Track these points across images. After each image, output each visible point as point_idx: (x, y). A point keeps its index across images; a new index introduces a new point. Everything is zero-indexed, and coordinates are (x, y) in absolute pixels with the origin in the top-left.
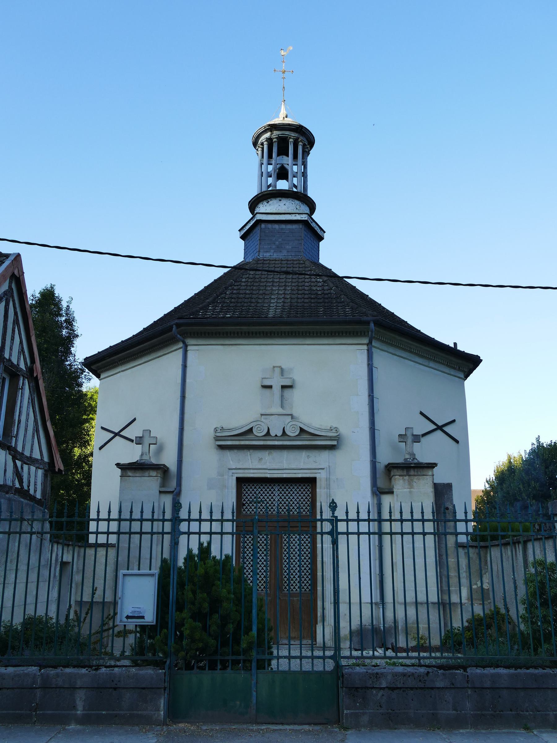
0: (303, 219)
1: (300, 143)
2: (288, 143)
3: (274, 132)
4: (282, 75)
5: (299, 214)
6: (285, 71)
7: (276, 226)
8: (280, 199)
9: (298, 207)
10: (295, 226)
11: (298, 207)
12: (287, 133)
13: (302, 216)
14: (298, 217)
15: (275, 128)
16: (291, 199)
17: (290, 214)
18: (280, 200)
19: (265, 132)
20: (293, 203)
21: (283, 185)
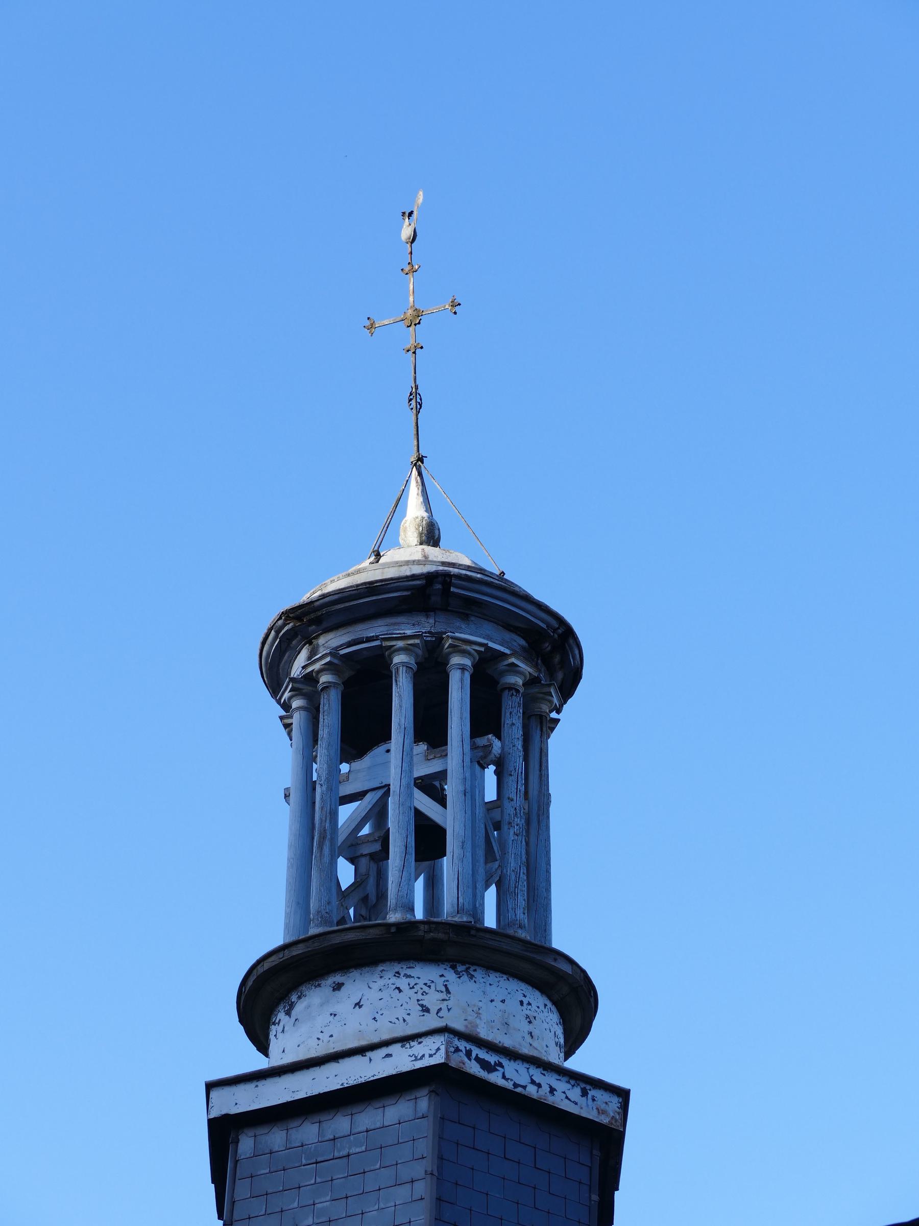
0: (427, 1062)
1: (456, 660)
2: (434, 679)
3: (322, 640)
4: (409, 337)
5: (404, 1040)
6: (418, 314)
7: (308, 1132)
8: (338, 978)
9: (433, 999)
10: (396, 1111)
11: (433, 999)
12: (376, 628)
13: (417, 1048)
14: (401, 1061)
15: (318, 621)
16: (389, 969)
17: (361, 1051)
18: (338, 987)
19: (508, 623)
20: (403, 983)
21: (410, 897)
